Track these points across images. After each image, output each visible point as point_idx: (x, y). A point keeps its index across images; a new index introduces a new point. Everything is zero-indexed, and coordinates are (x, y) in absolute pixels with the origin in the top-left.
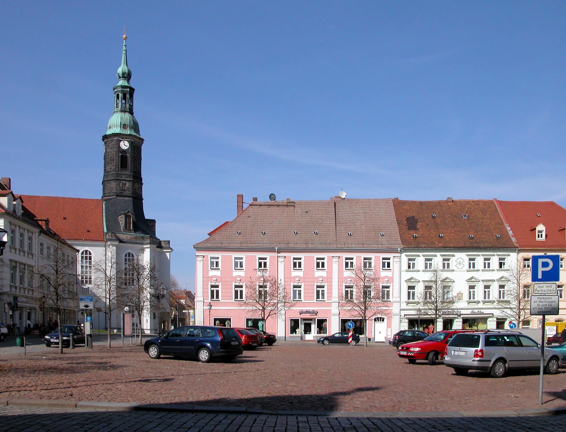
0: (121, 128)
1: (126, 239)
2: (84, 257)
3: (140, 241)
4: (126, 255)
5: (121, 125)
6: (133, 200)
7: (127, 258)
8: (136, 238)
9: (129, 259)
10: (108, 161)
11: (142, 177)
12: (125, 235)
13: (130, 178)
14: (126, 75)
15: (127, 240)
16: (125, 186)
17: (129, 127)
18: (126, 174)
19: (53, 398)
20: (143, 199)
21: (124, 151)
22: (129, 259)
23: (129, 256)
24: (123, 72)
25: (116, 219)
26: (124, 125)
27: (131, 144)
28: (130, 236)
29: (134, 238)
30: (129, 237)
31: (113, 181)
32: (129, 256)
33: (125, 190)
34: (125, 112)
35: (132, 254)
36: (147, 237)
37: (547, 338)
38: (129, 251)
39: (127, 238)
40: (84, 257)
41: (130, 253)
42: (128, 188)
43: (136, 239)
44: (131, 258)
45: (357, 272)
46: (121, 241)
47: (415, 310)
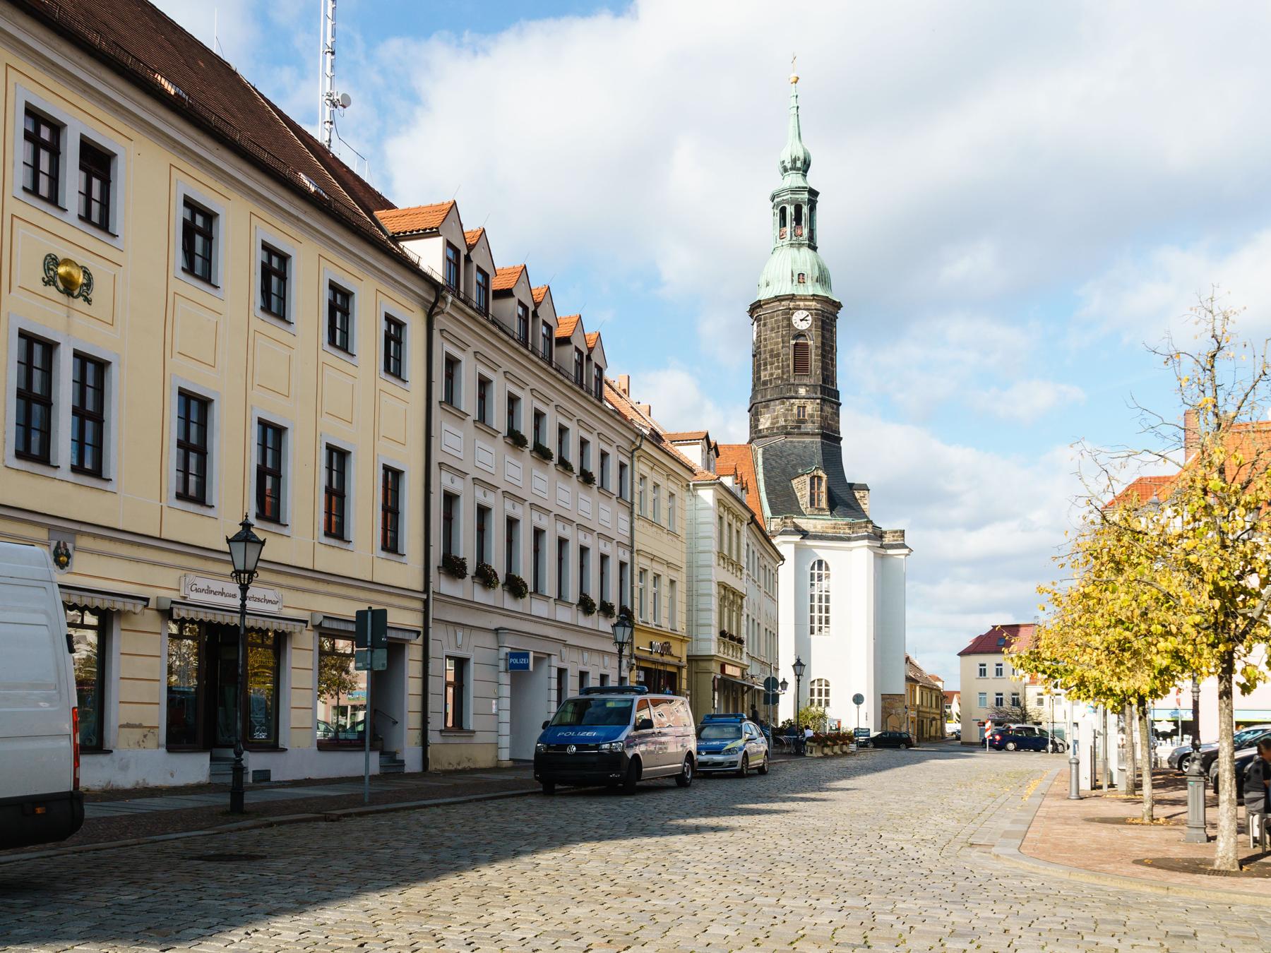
1: (813, 530)
5: (793, 276)
6: (822, 443)
7: (816, 571)
10: (766, 359)
13: (816, 393)
14: (799, 164)
16: (804, 412)
17: (809, 280)
18: (806, 385)
21: (800, 334)
24: (793, 157)
25: (788, 486)
26: (799, 275)
28: (822, 522)
31: (777, 402)
33: (804, 422)
34: (800, 245)
36: (861, 523)
42: (812, 416)
46: (805, 534)
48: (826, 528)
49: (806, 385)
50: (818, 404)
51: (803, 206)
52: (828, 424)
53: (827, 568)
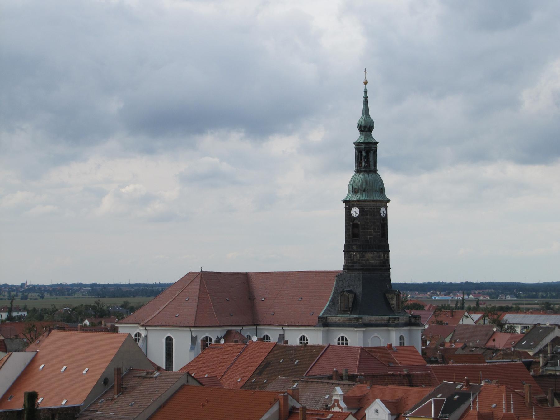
0: (353, 193)
1: (339, 322)
2: (342, 342)
3: (354, 323)
4: (339, 340)
7: (341, 342)
8: (349, 320)
9: (343, 344)
11: (389, 243)
12: (338, 318)
15: (340, 323)
18: (356, 245)
19: (140, 324)
20: (390, 268)
22: (343, 344)
23: (343, 340)
24: (360, 126)
27: (361, 209)
28: (342, 318)
29: (348, 321)
30: (342, 319)
32: (343, 340)
35: (210, 338)
37: (196, 348)
38: (342, 334)
39: (339, 320)
40: (342, 342)
41: (208, 337)
43: (349, 320)
44: (345, 342)
45: (23, 333)
47: (483, 392)
48: (345, 320)
49: (356, 245)
50: (361, 254)
51: (362, 151)
52: (370, 262)
53: (346, 340)
